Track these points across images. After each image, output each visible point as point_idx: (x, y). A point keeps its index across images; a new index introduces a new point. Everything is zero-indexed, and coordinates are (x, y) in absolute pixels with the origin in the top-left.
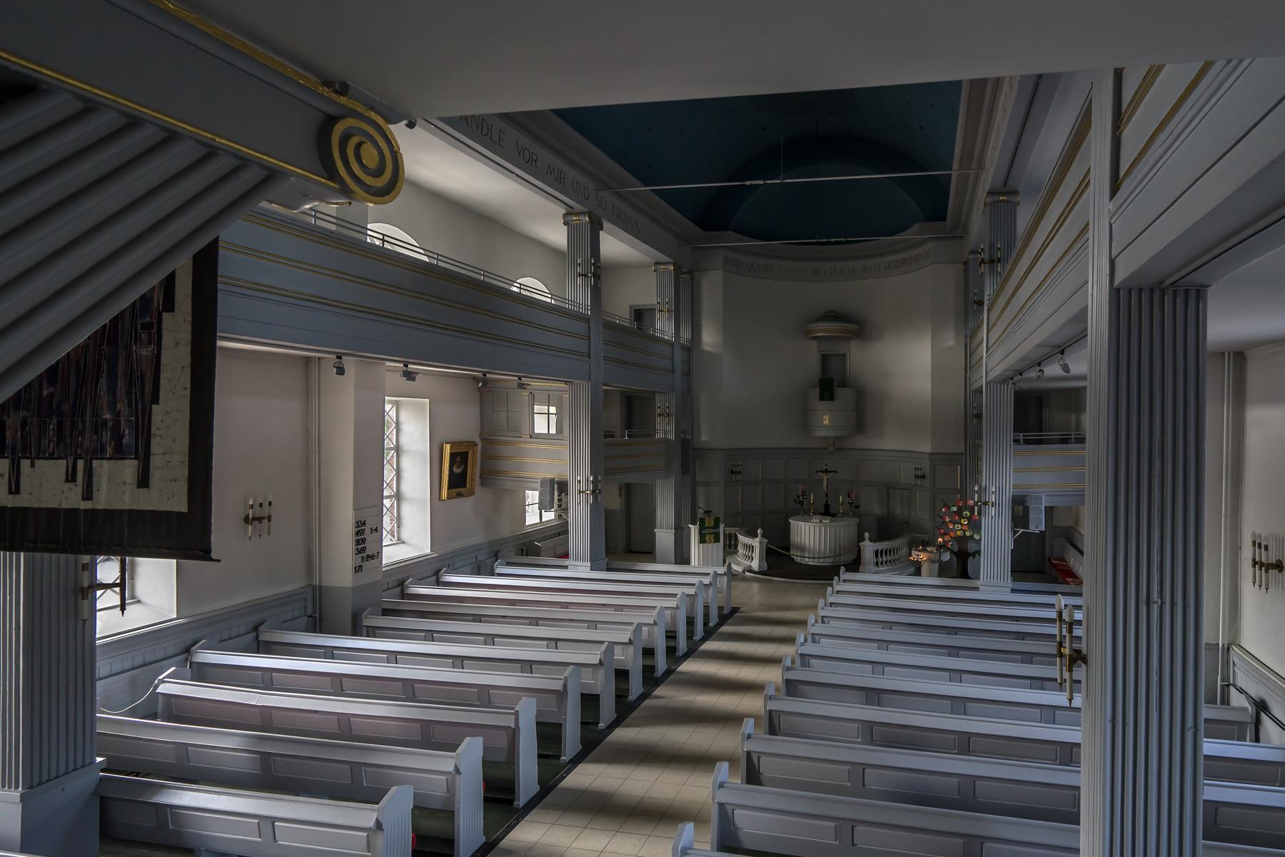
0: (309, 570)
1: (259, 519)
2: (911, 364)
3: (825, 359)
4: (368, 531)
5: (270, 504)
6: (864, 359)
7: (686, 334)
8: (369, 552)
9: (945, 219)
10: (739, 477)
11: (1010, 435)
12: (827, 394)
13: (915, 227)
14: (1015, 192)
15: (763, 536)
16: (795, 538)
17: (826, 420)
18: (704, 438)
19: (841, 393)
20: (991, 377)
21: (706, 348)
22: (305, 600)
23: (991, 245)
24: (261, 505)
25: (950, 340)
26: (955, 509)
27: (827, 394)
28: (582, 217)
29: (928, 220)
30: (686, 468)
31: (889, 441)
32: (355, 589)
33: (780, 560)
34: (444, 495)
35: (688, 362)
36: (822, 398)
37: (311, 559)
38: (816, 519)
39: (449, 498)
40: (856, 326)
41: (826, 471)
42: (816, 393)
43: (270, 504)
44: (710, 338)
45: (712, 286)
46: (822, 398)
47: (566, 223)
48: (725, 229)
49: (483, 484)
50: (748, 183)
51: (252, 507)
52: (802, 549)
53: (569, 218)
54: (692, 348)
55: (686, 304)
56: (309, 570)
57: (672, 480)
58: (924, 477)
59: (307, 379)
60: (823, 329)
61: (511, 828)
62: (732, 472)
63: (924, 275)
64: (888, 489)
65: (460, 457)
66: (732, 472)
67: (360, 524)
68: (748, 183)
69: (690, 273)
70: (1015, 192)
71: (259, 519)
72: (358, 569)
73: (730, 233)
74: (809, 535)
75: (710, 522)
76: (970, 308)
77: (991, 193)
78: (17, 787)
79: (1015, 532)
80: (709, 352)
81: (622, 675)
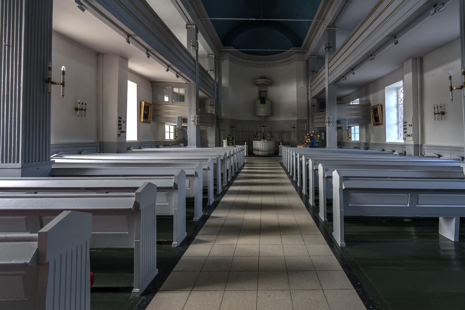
0: (98, 135)
1: (82, 110)
2: (290, 93)
3: (260, 92)
4: (122, 122)
5: (86, 104)
6: (272, 91)
7: (217, 80)
8: (123, 130)
9: (300, 46)
10: (234, 129)
11: (336, 102)
12: (263, 102)
13: (292, 48)
14: (335, 27)
15: (247, 144)
16: (254, 147)
17: (262, 110)
18: (223, 115)
19: (267, 102)
20: (330, 82)
21: (224, 85)
22: (97, 147)
23: (328, 43)
24: (82, 104)
25: (302, 84)
26: (308, 134)
27: (263, 102)
28: (193, 26)
29: (294, 46)
30: (218, 126)
31: (281, 118)
32: (118, 143)
33: (251, 153)
34: (142, 120)
35: (218, 89)
36: (261, 103)
37: (98, 132)
38: (262, 141)
39: (143, 122)
40: (271, 82)
41: (263, 126)
42: (259, 101)
43: (86, 104)
44: (225, 82)
45: (225, 64)
46: (261, 103)
47: (187, 28)
48: (230, 46)
49: (153, 120)
50: (255, 19)
51: (79, 103)
52: (258, 150)
53: (188, 26)
54: (219, 84)
55: (218, 70)
56: (98, 135)
57: (214, 128)
58: (294, 127)
59: (98, 62)
60: (261, 81)
61: (222, 198)
62: (232, 127)
63: (296, 65)
64: (282, 132)
65: (147, 108)
66: (232, 127)
67: (120, 118)
68: (250, 19)
69: (218, 60)
70: (335, 27)
71: (82, 110)
72: (119, 135)
73: (232, 47)
74: (259, 145)
75: (230, 138)
76: (311, 71)
77: (328, 27)
78: (18, 162)
79: (338, 131)
80: (224, 87)
81: (164, 223)
